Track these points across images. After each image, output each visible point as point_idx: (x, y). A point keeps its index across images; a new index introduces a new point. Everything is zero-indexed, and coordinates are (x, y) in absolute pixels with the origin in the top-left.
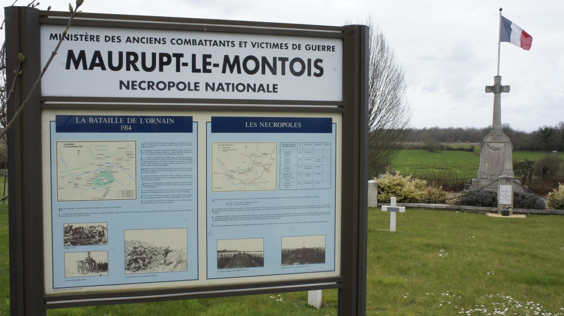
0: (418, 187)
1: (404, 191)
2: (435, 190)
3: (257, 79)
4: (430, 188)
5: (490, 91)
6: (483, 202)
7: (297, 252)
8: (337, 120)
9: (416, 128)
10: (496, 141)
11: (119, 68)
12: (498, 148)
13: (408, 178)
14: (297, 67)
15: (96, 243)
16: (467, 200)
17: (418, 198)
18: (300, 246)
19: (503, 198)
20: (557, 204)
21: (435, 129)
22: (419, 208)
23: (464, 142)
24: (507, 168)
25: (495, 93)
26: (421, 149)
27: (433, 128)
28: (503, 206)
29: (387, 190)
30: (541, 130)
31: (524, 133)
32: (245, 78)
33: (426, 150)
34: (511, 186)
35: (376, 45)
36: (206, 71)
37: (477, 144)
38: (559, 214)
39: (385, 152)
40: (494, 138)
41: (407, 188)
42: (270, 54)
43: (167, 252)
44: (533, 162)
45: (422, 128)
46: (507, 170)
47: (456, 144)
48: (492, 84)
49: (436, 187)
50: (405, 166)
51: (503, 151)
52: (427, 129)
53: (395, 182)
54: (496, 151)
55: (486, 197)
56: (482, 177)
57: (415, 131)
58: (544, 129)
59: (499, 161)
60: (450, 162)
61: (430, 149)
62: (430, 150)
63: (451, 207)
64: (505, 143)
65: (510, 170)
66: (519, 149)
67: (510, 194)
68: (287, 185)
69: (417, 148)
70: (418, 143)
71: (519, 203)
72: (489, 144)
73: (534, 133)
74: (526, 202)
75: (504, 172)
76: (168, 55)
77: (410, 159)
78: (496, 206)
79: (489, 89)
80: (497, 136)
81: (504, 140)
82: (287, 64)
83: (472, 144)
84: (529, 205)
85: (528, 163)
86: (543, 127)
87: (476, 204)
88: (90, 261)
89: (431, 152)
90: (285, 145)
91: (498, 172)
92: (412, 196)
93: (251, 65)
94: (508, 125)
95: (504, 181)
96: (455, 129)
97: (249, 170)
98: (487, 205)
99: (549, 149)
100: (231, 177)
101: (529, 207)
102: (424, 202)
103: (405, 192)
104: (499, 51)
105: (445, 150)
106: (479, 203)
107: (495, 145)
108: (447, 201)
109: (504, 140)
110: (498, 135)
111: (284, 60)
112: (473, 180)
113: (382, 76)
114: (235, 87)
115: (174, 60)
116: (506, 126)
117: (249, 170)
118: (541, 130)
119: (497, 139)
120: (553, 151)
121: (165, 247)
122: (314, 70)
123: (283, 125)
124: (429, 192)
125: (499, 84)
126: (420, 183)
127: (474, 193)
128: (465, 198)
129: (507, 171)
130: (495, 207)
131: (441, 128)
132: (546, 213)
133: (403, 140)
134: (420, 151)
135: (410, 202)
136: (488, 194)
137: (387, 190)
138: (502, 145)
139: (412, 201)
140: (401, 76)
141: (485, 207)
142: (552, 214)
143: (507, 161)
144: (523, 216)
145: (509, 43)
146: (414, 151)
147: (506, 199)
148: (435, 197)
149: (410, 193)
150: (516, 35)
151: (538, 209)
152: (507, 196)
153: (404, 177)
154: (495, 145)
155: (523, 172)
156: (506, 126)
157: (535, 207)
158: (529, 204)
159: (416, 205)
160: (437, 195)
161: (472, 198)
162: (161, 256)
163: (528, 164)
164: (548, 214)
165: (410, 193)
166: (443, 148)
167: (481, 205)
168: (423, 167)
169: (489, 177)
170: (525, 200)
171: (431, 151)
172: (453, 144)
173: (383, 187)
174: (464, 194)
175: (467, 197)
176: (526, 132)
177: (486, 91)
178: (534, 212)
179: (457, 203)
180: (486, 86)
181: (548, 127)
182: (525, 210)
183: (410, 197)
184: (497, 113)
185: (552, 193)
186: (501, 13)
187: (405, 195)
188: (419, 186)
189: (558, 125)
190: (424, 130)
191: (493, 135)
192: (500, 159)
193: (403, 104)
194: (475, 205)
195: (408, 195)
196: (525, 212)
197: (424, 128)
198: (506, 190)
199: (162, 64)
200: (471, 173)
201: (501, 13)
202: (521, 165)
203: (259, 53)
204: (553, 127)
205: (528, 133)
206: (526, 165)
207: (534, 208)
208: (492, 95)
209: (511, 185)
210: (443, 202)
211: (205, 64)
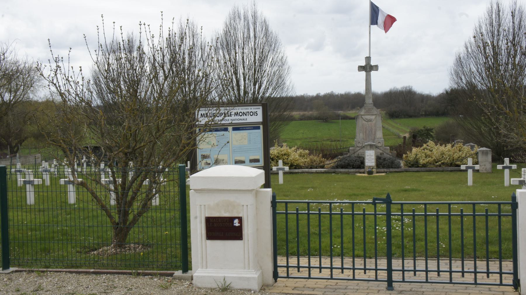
0: (302, 156)
1: (290, 159)
2: (315, 158)
3: (242, 117)
4: (311, 157)
5: (362, 70)
6: (353, 165)
7: (253, 160)
8: (261, 126)
9: (308, 94)
10: (368, 114)
11: (219, 116)
13: (293, 149)
14: (251, 114)
15: (208, 158)
16: (341, 164)
17: (302, 165)
18: (254, 158)
20: (410, 163)
21: (330, 95)
22: (303, 172)
25: (366, 71)
26: (314, 120)
27: (328, 94)
28: (369, 167)
29: (276, 160)
30: (447, 92)
31: (431, 95)
32: (239, 117)
33: (320, 121)
34: (374, 151)
35: (261, 30)
36: (231, 116)
38: (411, 171)
39: (273, 127)
41: (293, 157)
42: (245, 111)
43: (223, 160)
44: (432, 129)
45: (314, 94)
46: (378, 139)
47: (354, 112)
48: (363, 64)
49: (316, 155)
50: (297, 139)
51: (374, 122)
52: (320, 95)
53: (283, 153)
55: (355, 161)
56: (358, 145)
57: (306, 97)
58: (450, 90)
59: (372, 131)
60: (347, 133)
61: (324, 119)
62: (325, 120)
63: (328, 170)
65: (381, 138)
66: (423, 115)
67: (374, 157)
68: (250, 143)
69: (310, 118)
70: (311, 112)
71: (381, 164)
74: (386, 163)
76: (222, 113)
77: (302, 131)
78: (364, 168)
79: (361, 68)
80: (369, 109)
81: (375, 113)
82: (249, 113)
84: (389, 166)
86: (449, 88)
87: (348, 167)
88: (207, 163)
89: (325, 122)
90: (249, 133)
92: (297, 163)
93: (241, 114)
94: (410, 87)
95: (369, 147)
96: (352, 94)
97: (241, 140)
98: (356, 167)
100: (237, 142)
101: (388, 167)
102: (307, 168)
103: (291, 161)
105: (339, 119)
106: (350, 166)
107: (368, 117)
108: (325, 166)
109: (375, 113)
110: (370, 109)
111: (248, 112)
112: (351, 148)
113: (268, 58)
114: (237, 120)
115: (223, 114)
117: (241, 140)
121: (223, 159)
122: (255, 114)
123: (249, 128)
124: (311, 159)
125: (369, 64)
126: (304, 152)
127: (346, 158)
128: (340, 163)
130: (362, 169)
131: (337, 94)
132: (401, 171)
133: (292, 109)
134: (314, 121)
135: (295, 168)
136: (357, 158)
137: (276, 160)
138: (373, 117)
139: (297, 168)
140: (285, 58)
141: (355, 169)
142: (405, 171)
144: (383, 174)
145: (376, 26)
146: (306, 121)
147: (371, 161)
148: (317, 164)
149: (296, 161)
150: (381, 19)
151: (395, 168)
153: (290, 148)
154: (368, 117)
157: (393, 166)
158: (389, 165)
159: (300, 170)
160: (318, 162)
161: (345, 162)
162: (222, 161)
163: (426, 131)
164: (403, 172)
165: (296, 161)
166: (338, 117)
167: (351, 167)
168: (317, 140)
170: (386, 162)
171: (326, 121)
172: (351, 112)
173: (273, 157)
174: (339, 159)
175: (341, 161)
176: (432, 95)
177: (358, 70)
178: (392, 171)
179: (333, 168)
180: (359, 66)
182: (385, 170)
183: (296, 164)
184: (368, 89)
185: (406, 155)
187: (291, 163)
188: (302, 155)
190: (318, 97)
191: (365, 109)
192: (372, 129)
193: (288, 83)
194: (347, 168)
195: (294, 163)
196: (386, 171)
197: (317, 94)
198: (370, 154)
199: (221, 115)
202: (419, 133)
203: (242, 111)
205: (434, 95)
206: (425, 133)
207: (392, 168)
208: (363, 73)
209: (373, 150)
210: (323, 167)
211: (230, 114)
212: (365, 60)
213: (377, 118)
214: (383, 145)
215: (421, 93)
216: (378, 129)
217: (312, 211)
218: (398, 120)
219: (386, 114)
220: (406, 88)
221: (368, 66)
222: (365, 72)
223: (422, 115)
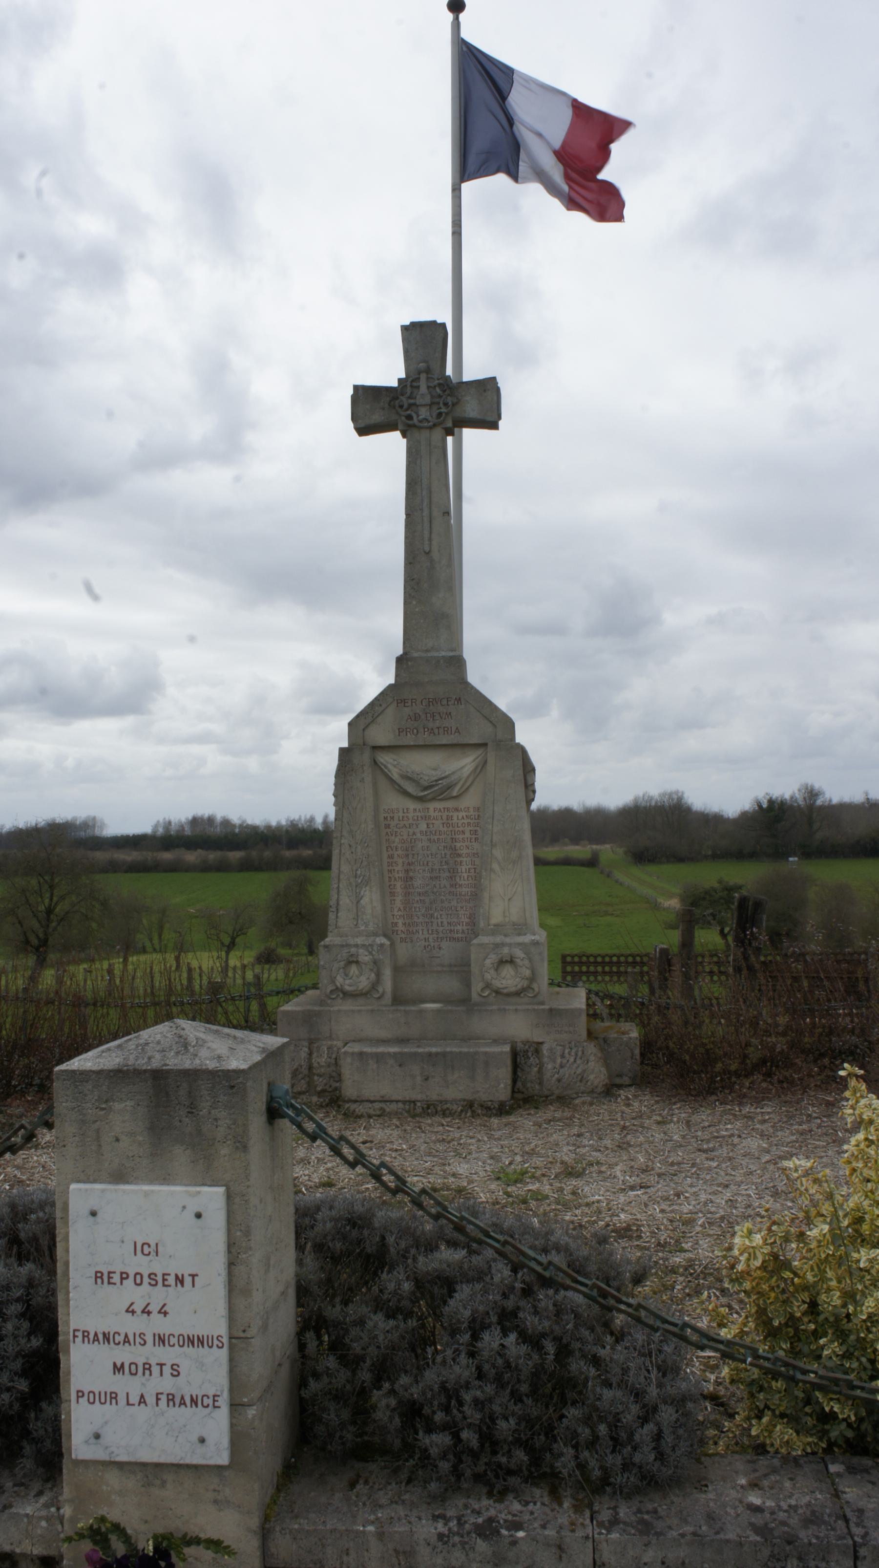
10: (425, 738)
12: (444, 782)
19: (118, 1369)
23: (577, 844)
24: (497, 917)
31: (722, 816)
37: (608, 846)
40: (416, 717)
46: (498, 929)
51: (470, 801)
54: (432, 806)
64: (479, 752)
65: (520, 928)
72: (385, 759)
73: (744, 815)
75: (481, 945)
83: (594, 847)
85: (727, 889)
86: (764, 797)
91: (445, 944)
94: (680, 794)
99: (779, 854)
104: (454, 233)
116: (675, 797)
118: (760, 806)
119: (430, 725)
120: (791, 859)
125: (428, 371)
129: (499, 939)
138: (466, 763)
143: (495, 866)
147: (167, 1384)
152: (161, 1340)
155: (713, 916)
156: (675, 797)
163: (726, 892)
169: (387, 985)
172: (550, 849)
176: (726, 816)
181: (774, 797)
186: (456, 26)
189: (796, 792)
198: (143, 1249)
200: (585, 925)
201: (456, 26)
204: (787, 796)
212: (405, 340)
213: (490, 768)
214: (532, 979)
215: (703, 809)
216: (498, 853)
217: (502, 1052)
218: (653, 868)
219: (626, 853)
220: (670, 795)
221: (423, 384)
222: (404, 435)
223: (706, 857)
